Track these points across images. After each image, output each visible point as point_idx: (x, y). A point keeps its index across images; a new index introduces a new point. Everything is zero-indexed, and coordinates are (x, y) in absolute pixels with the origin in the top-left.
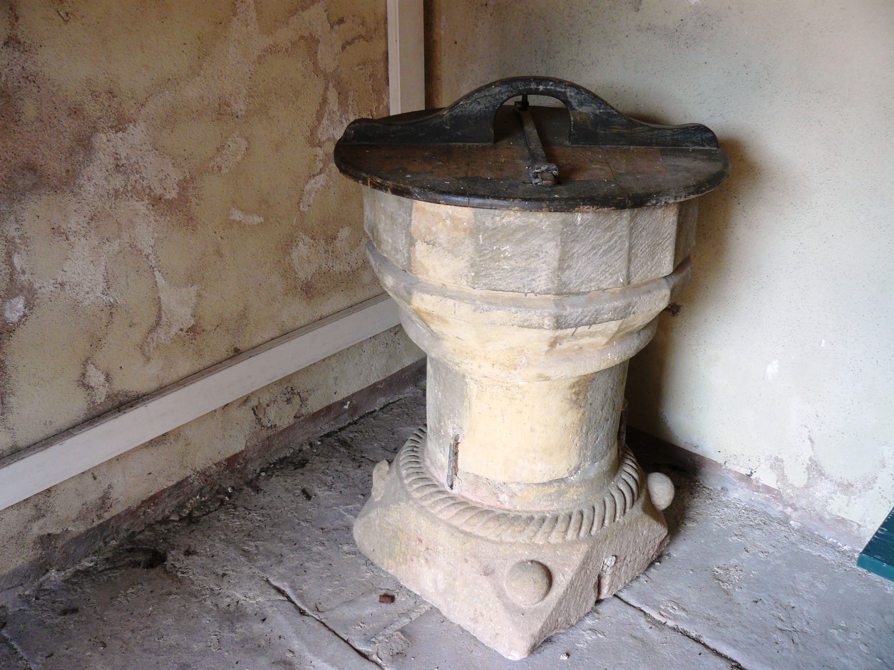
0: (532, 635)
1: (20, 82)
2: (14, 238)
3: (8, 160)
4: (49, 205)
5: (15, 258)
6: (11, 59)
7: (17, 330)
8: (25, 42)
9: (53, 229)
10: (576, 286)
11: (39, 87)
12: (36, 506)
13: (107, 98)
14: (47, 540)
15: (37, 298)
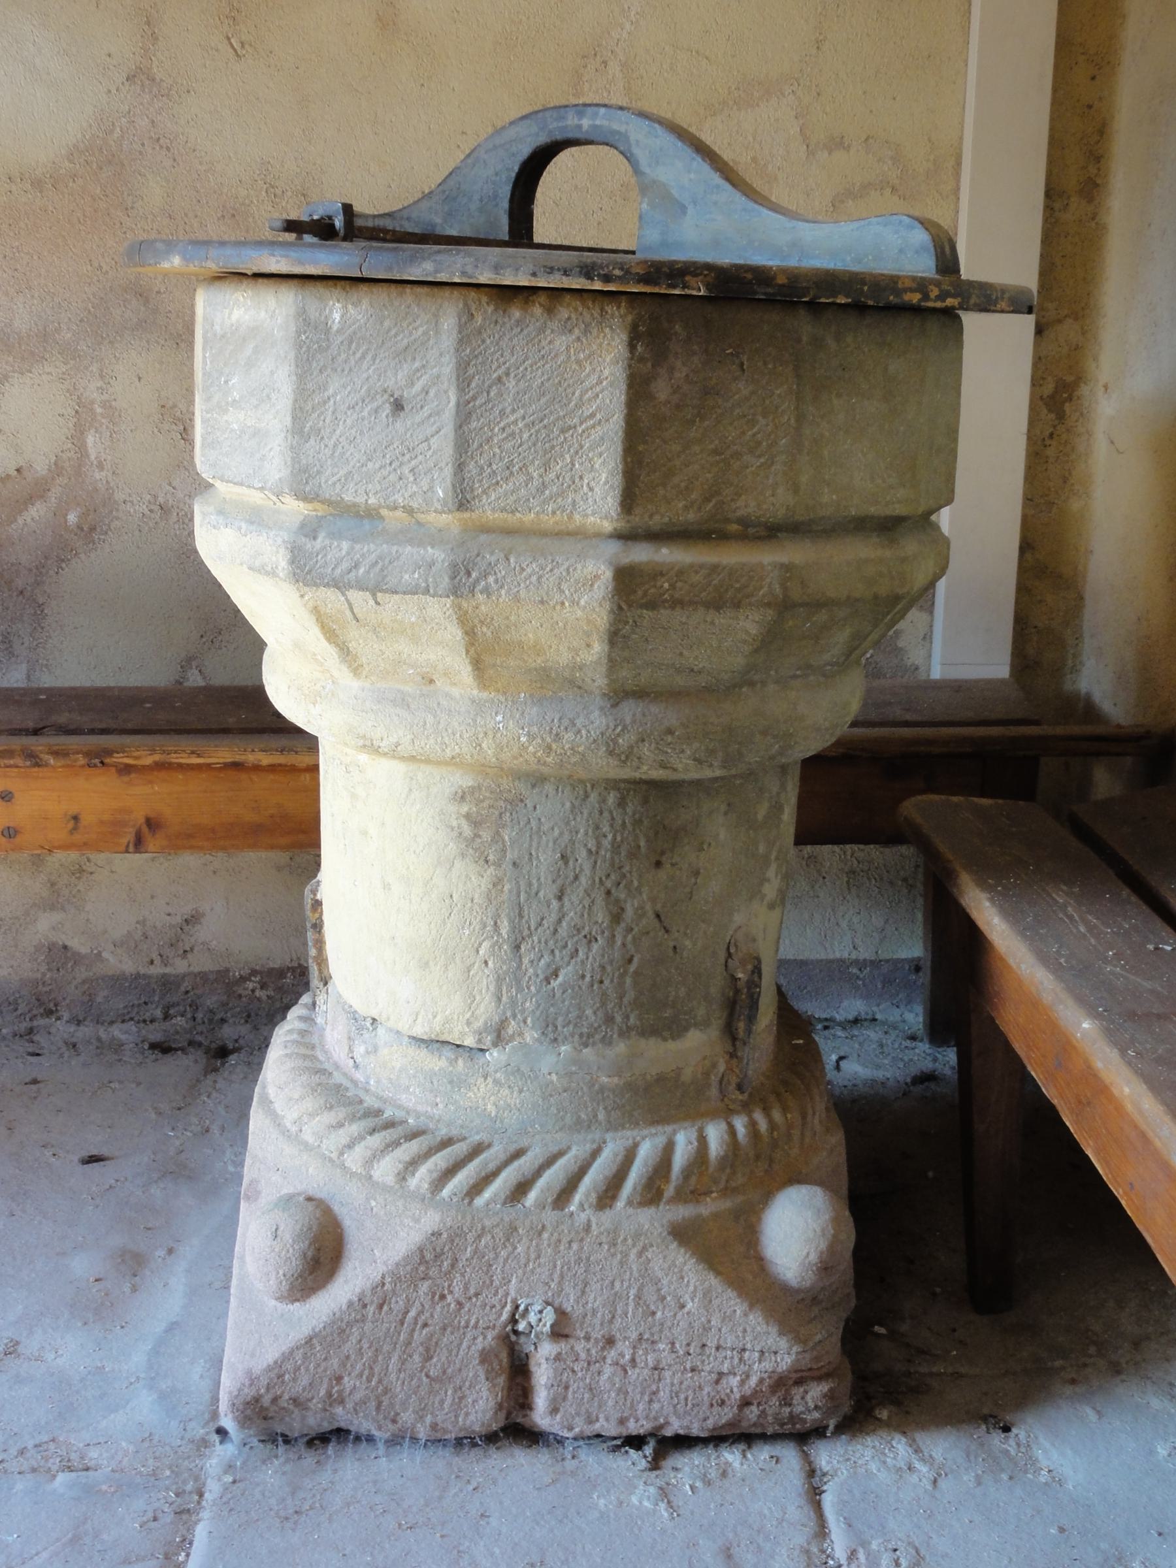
0: (249, 1372)
1: (143, 145)
2: (92, 402)
3: (104, 270)
4: (161, 363)
5: (90, 437)
6: (135, 104)
7: (73, 562)
8: (161, 80)
9: (163, 406)
10: (334, 484)
11: (175, 160)
12: (53, 885)
13: (295, 203)
14: (59, 955)
15: (117, 518)
